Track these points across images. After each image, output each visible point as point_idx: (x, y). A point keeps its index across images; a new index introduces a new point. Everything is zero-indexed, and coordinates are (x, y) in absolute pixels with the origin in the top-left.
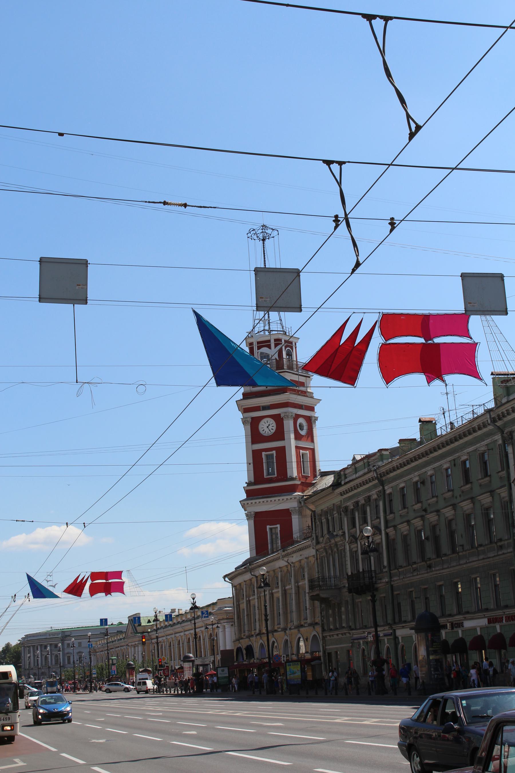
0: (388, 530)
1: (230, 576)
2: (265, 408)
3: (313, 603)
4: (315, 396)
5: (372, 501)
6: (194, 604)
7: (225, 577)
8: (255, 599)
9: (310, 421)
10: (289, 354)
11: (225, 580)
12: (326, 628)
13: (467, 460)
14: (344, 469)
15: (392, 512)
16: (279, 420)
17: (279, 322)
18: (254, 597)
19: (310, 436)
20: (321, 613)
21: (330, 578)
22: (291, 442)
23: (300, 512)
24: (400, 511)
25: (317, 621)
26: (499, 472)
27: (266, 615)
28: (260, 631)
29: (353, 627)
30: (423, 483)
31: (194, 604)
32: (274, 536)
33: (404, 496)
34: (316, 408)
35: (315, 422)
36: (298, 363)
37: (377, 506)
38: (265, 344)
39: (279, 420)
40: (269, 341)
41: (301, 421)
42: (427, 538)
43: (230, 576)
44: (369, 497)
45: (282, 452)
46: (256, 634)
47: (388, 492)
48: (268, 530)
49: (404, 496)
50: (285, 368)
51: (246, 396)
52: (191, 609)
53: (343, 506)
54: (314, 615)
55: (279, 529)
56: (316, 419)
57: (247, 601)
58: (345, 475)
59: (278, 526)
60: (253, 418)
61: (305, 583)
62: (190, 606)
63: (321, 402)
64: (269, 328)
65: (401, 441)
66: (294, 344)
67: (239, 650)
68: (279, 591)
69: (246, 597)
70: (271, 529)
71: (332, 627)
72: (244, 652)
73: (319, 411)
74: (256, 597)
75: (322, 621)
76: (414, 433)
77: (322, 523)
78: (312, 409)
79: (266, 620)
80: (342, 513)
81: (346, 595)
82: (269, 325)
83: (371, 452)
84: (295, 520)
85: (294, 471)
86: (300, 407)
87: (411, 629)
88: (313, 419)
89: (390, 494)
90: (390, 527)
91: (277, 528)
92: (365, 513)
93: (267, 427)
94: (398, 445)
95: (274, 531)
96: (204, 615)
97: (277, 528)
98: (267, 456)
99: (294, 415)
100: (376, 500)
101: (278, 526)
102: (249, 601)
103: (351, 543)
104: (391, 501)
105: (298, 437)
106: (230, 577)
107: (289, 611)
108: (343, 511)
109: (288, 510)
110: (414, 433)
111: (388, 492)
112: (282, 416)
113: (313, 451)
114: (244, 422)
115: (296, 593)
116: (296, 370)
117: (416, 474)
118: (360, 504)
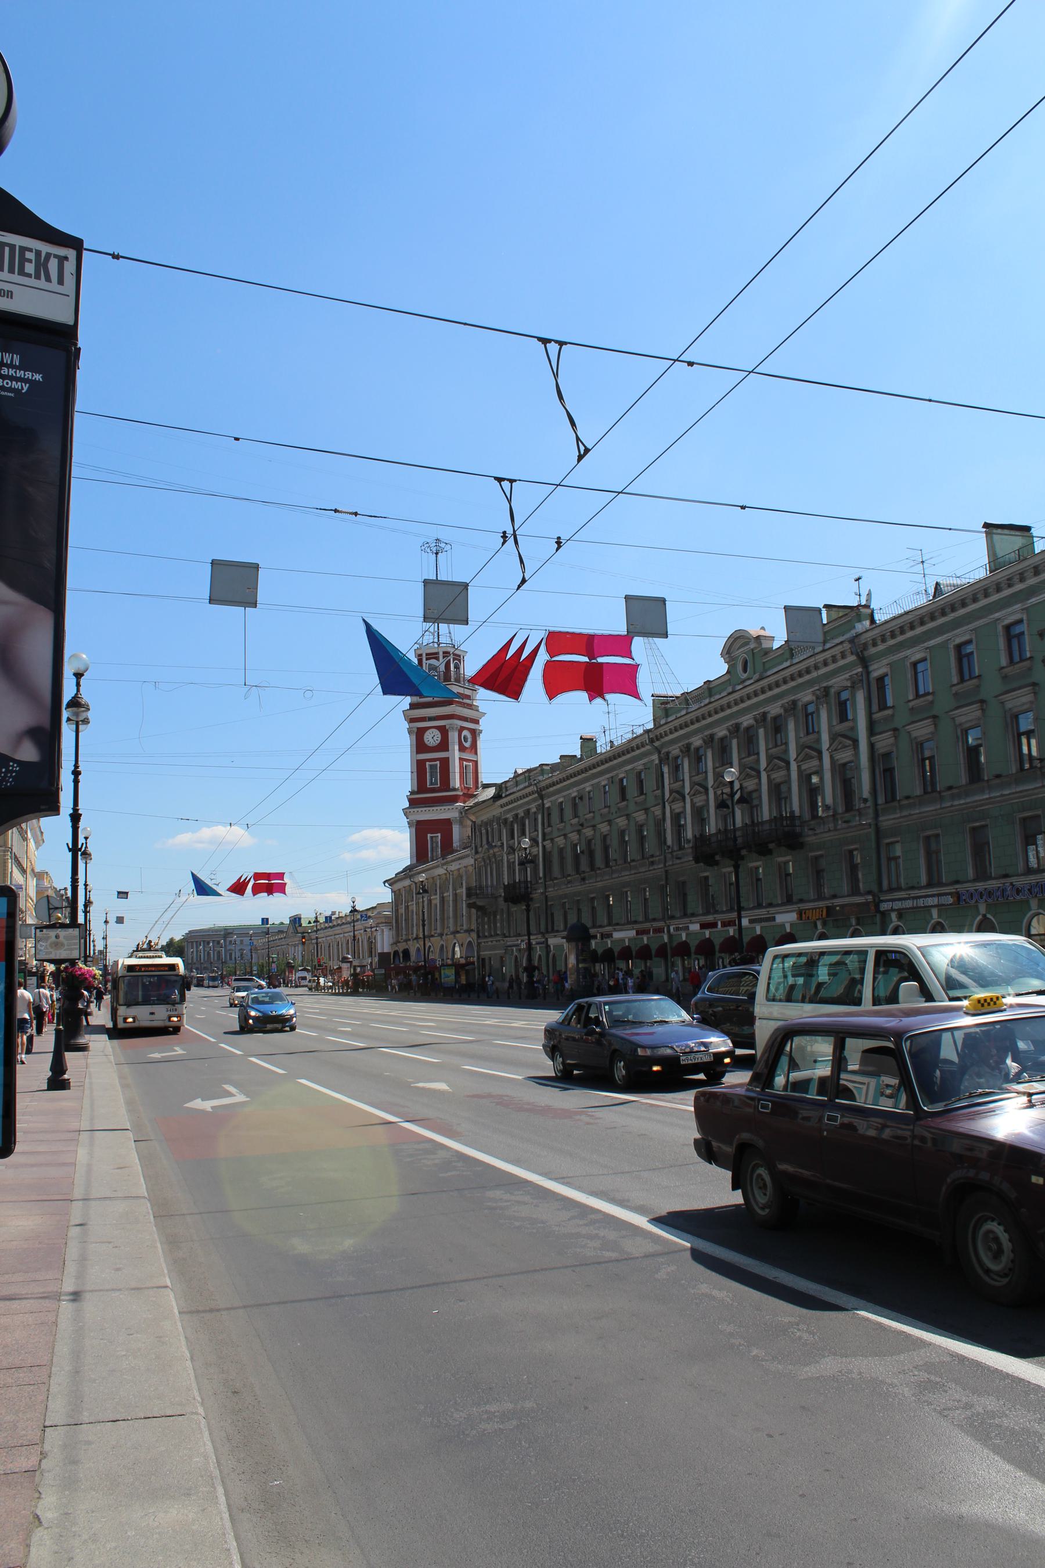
0: (545, 843)
2: (431, 719)
9: (475, 734)
10: (457, 667)
16: (444, 731)
19: (474, 748)
21: (487, 887)
22: (455, 754)
23: (461, 822)
30: (581, 798)
37: (536, 819)
39: (444, 731)
40: (437, 653)
41: (465, 733)
45: (445, 763)
49: (562, 810)
60: (418, 729)
65: (562, 757)
67: (396, 953)
70: (432, 838)
73: (483, 725)
79: (424, 925)
84: (456, 829)
86: (465, 719)
87: (563, 938)
93: (432, 738)
98: (431, 766)
104: (549, 815)
105: (462, 749)
113: (476, 763)
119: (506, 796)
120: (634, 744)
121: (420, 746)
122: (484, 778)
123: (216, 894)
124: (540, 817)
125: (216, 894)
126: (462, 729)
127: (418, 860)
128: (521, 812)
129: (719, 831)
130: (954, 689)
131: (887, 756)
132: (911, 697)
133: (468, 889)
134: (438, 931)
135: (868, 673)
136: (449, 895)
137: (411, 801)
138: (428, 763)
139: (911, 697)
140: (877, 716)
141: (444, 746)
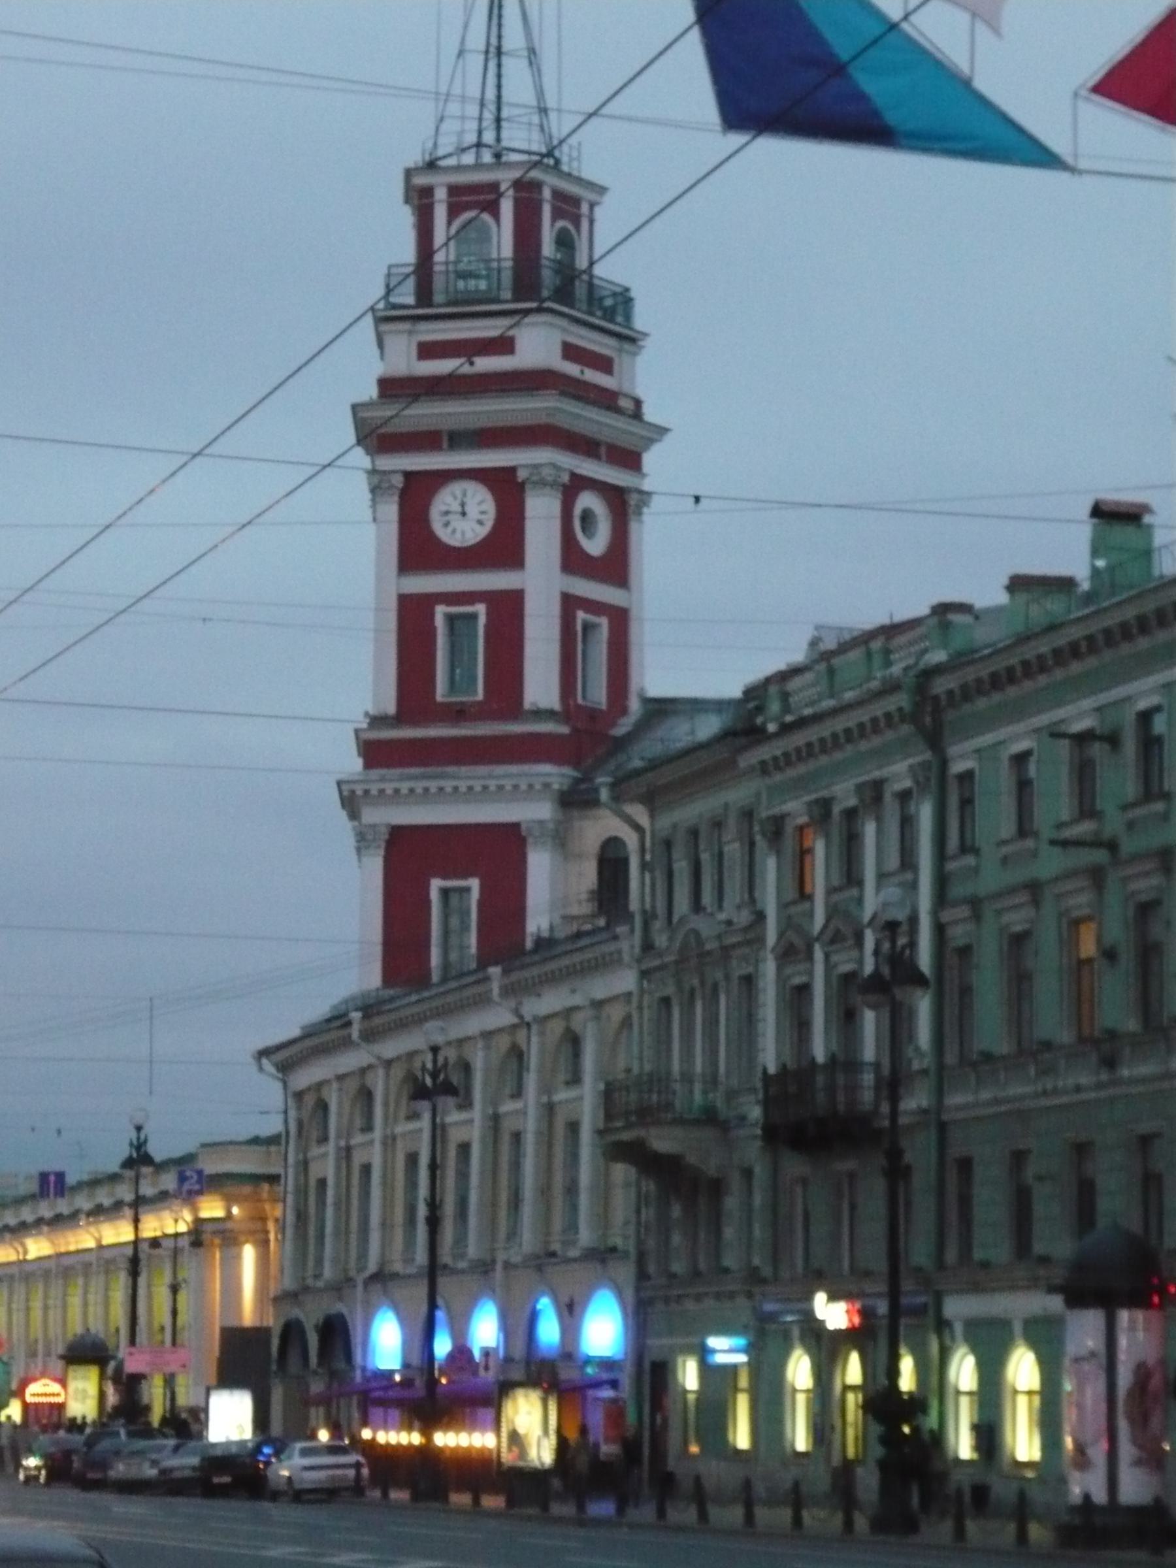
0: (946, 916)
1: (280, 1056)
2: (459, 439)
3: (607, 1169)
4: (651, 414)
5: (888, 797)
6: (140, 1146)
7: (264, 1053)
8: (371, 1142)
9: (623, 505)
10: (565, 242)
11: (261, 1069)
12: (652, 1269)
13: (1158, 709)
14: (783, 677)
15: (966, 848)
16: (507, 488)
17: (536, 119)
18: (322, 1150)
19: (615, 566)
20: (638, 1212)
21: (687, 1078)
22: (540, 580)
23: (561, 840)
24: (1004, 842)
25: (618, 1241)
26: (1004, 842)
27: (434, 1205)
28: (382, 1264)
29: (767, 1271)
30: (1113, 740)
31: (140, 1146)
32: (454, 922)
33: (1023, 786)
34: (649, 460)
35: (640, 514)
36: (596, 281)
37: (907, 823)
38: (473, 198)
39: (507, 488)
40: (494, 187)
41: (587, 500)
42: (1110, 955)
43: (280, 1056)
44: (878, 786)
45: (508, 610)
46: (367, 1274)
47: (958, 767)
48: (434, 895)
49: (1023, 786)
50: (545, 293)
51: (390, 387)
52: (129, 1163)
53: (764, 814)
54: (603, 1219)
55: (475, 894)
56: (645, 497)
57: (338, 1149)
58: (785, 696)
59: (474, 884)
60: (408, 475)
61: (585, 1102)
62: (124, 1151)
63: (668, 439)
64: (498, 140)
65: (1018, 584)
66: (585, 208)
67: (292, 1331)
68: (471, 1121)
69: (338, 1137)
70: (445, 893)
71: (677, 1267)
72: (313, 1340)
73: (659, 467)
74: (377, 1134)
75: (640, 1242)
76: (1070, 554)
77: (721, 855)
78: (630, 460)
79: (434, 1222)
80: (758, 838)
81: (752, 1152)
82: (498, 128)
83: (903, 614)
84: (540, 865)
85: (541, 685)
86: (587, 446)
87: (1052, 1290)
88: (633, 499)
89: (967, 777)
90: (956, 904)
91: (468, 890)
92: (852, 840)
93: (463, 515)
94: (1003, 598)
95: (454, 900)
96: (186, 1187)
97: (468, 890)
98: (451, 619)
99: (566, 478)
100: (904, 797)
101: (474, 884)
102: (349, 1149)
103: (833, 941)
104: (967, 802)
105: (573, 559)
106: (284, 1058)
107: (1076, 1098)
108: (764, 835)
109: (516, 826)
110: (1070, 554)
111: (958, 767)
112: (522, 475)
113: (620, 618)
114: (378, 485)
115: (539, 1133)
116: (584, 307)
117: (1088, 703)
118: (836, 810)
119: (786, 729)
120: (1029, 652)
121: (418, 547)
122: (659, 674)
123: (990, 137)
124: (925, 814)
125: (990, 137)
126: (577, 484)
127: (391, 974)
128: (844, 793)
129: (784, 1070)
130: (1005, 850)
131: (965, 952)
132: (1065, 816)
133: (609, 1094)
134: (473, 1250)
135: (944, 764)
136: (525, 1113)
137: (374, 753)
138: (440, 611)
139: (1065, 816)
140: (951, 866)
141: (504, 545)
